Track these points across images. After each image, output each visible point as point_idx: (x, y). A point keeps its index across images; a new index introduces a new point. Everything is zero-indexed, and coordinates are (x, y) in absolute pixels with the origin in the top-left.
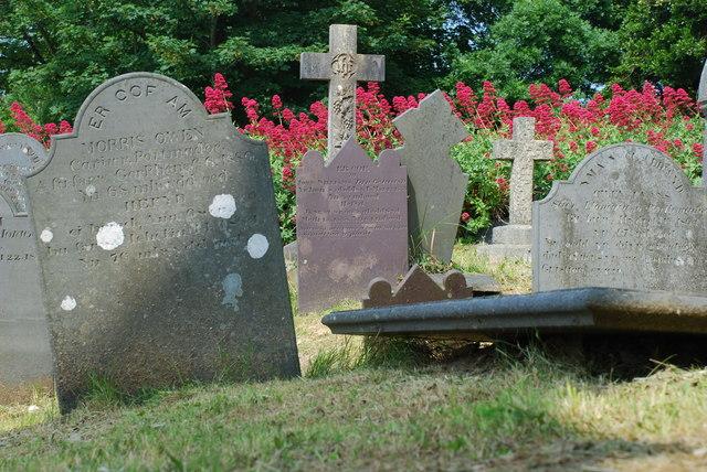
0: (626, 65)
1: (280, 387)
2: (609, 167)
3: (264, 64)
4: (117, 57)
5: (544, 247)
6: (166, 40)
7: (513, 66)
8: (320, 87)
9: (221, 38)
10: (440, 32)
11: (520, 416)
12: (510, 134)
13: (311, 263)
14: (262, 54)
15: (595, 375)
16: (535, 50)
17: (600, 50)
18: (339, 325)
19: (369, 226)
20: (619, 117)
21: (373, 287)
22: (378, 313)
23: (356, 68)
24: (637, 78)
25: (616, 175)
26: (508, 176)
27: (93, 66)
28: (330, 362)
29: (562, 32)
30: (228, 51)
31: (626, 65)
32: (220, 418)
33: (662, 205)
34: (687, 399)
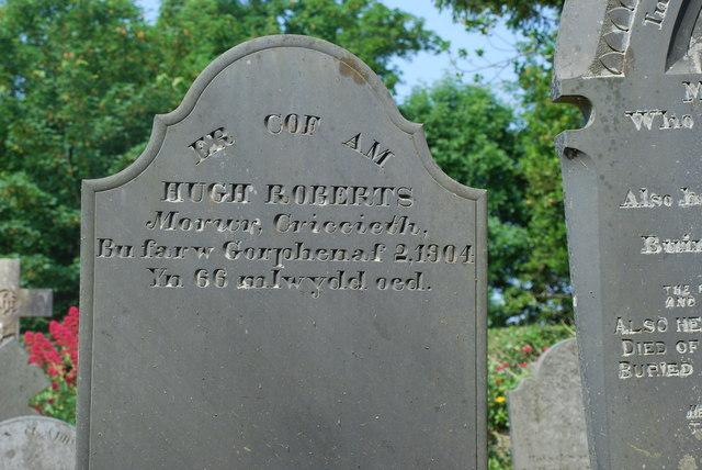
23: (19, 304)
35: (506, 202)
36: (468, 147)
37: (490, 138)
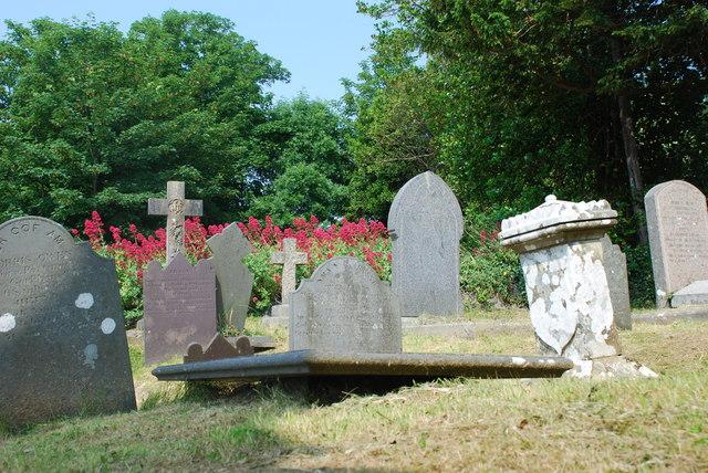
0: (353, 206)
1: (120, 419)
2: (334, 271)
3: (129, 204)
4: (28, 200)
5: (297, 320)
6: (62, 191)
7: (287, 205)
8: (160, 221)
9: (100, 188)
10: (243, 184)
11: (256, 433)
12: (281, 249)
13: (153, 333)
14: (127, 198)
15: (311, 402)
16: (300, 196)
17: (338, 197)
18: (163, 375)
19: (191, 308)
20: (347, 238)
21: (191, 347)
22: (196, 365)
23: (184, 208)
24: (360, 213)
25: (338, 275)
26: (281, 274)
27: (12, 207)
28: (157, 399)
29: (316, 186)
30: (103, 196)
31: (353, 206)
32: (72, 444)
33: (364, 293)
34: (356, 416)
35: (336, 171)
36: (314, 138)
37: (327, 134)
